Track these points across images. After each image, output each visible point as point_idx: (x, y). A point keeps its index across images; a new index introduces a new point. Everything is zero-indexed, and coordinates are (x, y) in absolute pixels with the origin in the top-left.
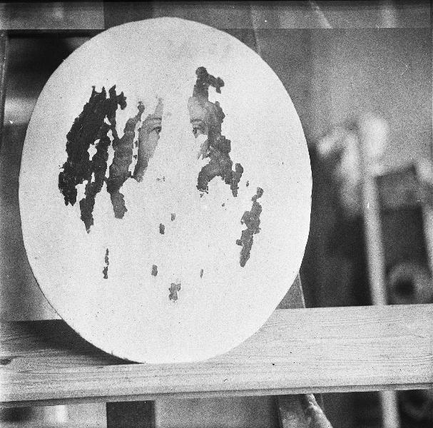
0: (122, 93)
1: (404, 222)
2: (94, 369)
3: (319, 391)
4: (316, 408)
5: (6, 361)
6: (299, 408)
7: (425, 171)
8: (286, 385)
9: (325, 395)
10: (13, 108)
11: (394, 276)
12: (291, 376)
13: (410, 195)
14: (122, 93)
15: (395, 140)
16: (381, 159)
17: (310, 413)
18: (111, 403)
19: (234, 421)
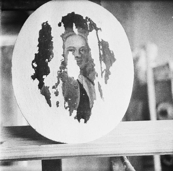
0: (79, 121)
1: (163, 85)
2: (37, 146)
3: (161, 154)
4: (127, 161)
5: (2, 143)
9: (129, 157)
11: (159, 109)
13: (167, 75)
14: (79, 121)
17: (125, 164)
18: (43, 160)
19: (95, 166)
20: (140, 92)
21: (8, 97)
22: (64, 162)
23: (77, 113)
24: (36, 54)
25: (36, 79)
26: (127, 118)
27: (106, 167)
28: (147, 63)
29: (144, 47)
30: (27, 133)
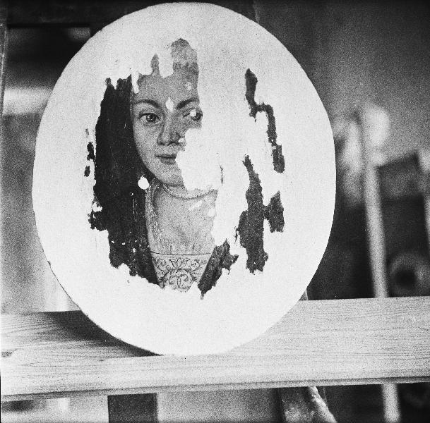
1: (402, 210)
3: (399, 382)
4: (320, 401)
6: (301, 400)
7: (425, 161)
10: (19, 99)
11: (396, 264)
13: (412, 185)
15: (396, 127)
16: (382, 150)
17: (313, 406)
19: (235, 412)
20: (348, 220)
21: (21, 238)
22: (161, 400)
23: (110, 239)
27: (263, 414)
28: (364, 156)
29: (356, 117)
30: (76, 327)
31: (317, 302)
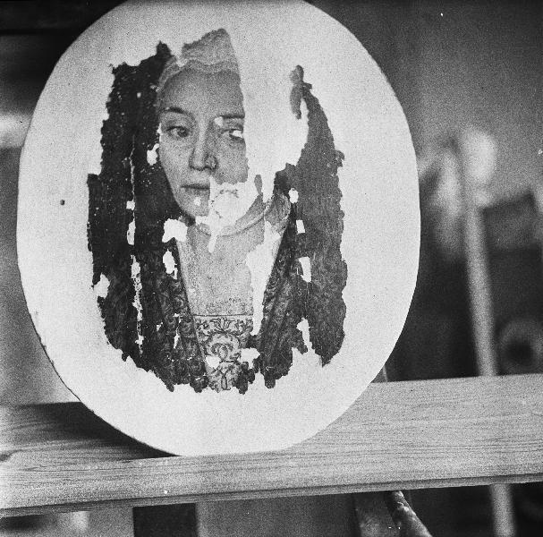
3: (410, 487)
8: (471, 474)
11: (506, 337)
12: (347, 470)
13: (527, 233)
16: (490, 185)
17: (401, 516)
22: (203, 512)
24: (104, 121)
25: (129, 357)
26: (323, 365)
28: (463, 194)
30: (77, 425)
31: (407, 385)
